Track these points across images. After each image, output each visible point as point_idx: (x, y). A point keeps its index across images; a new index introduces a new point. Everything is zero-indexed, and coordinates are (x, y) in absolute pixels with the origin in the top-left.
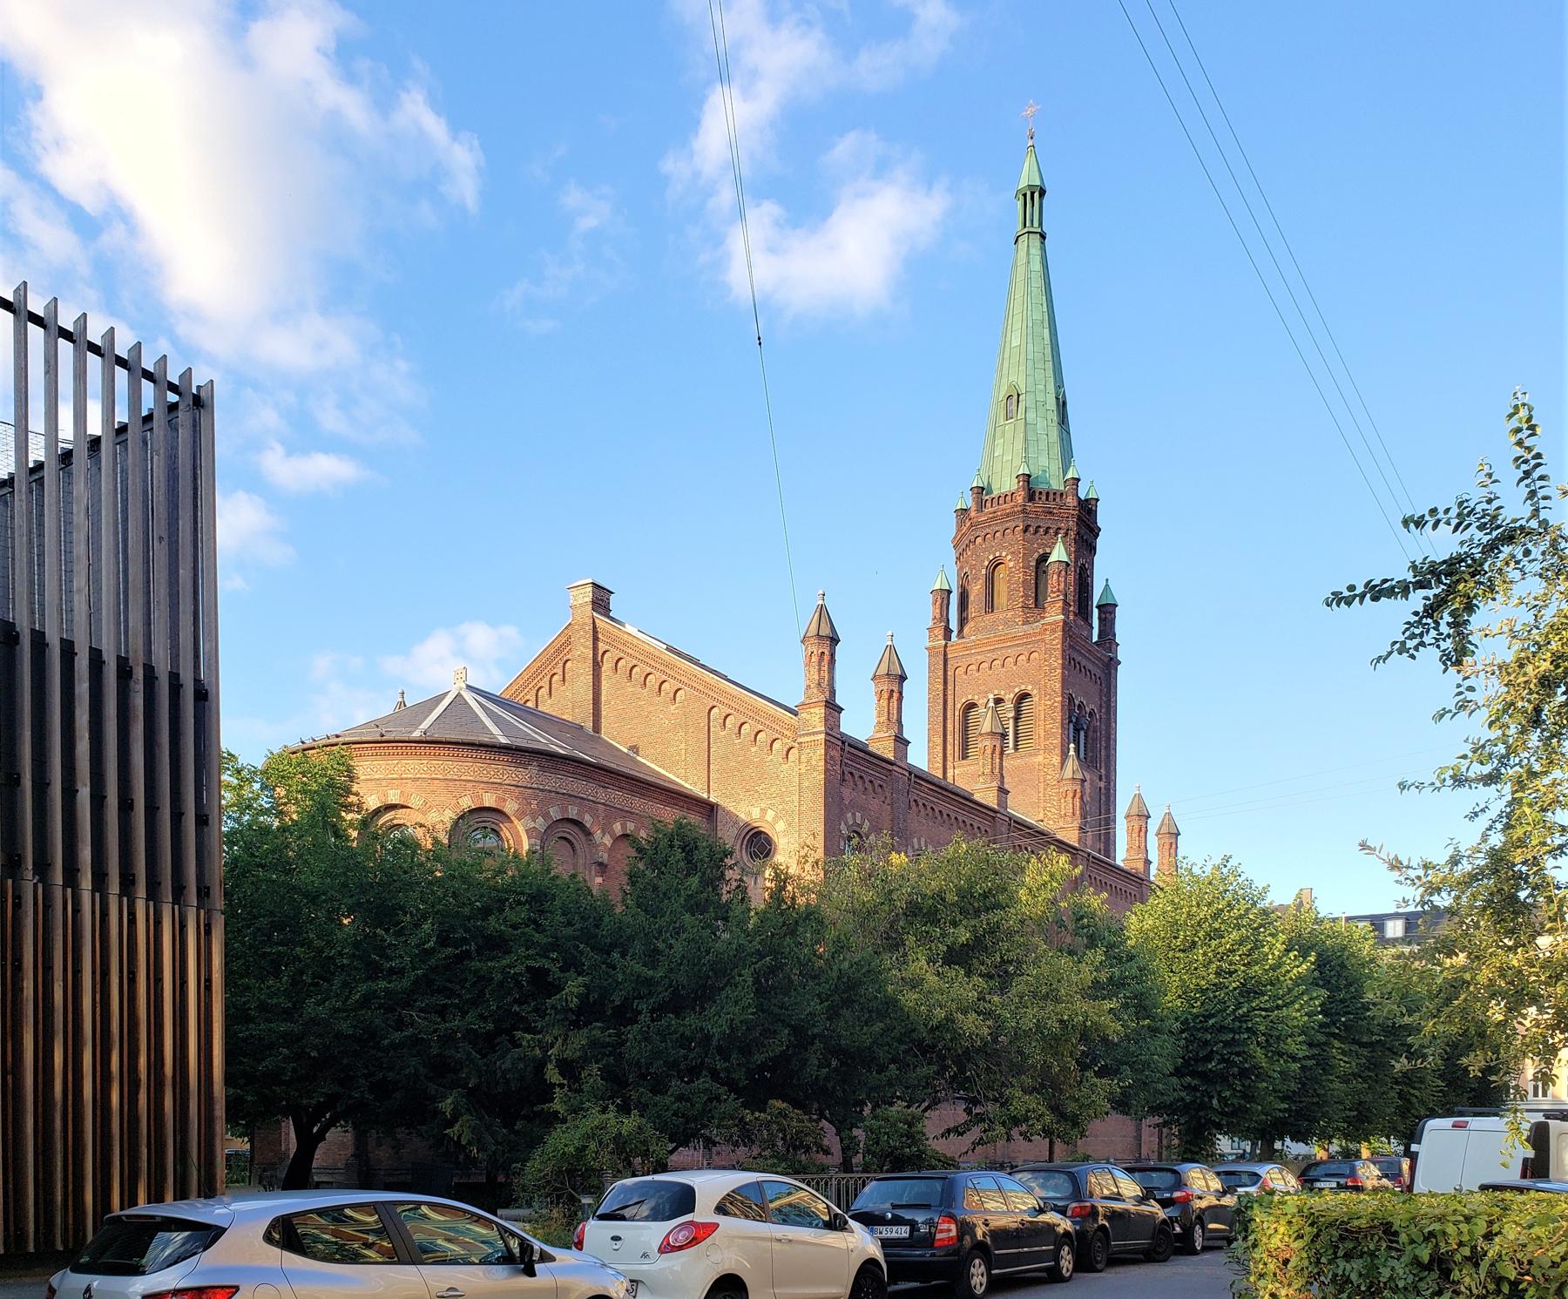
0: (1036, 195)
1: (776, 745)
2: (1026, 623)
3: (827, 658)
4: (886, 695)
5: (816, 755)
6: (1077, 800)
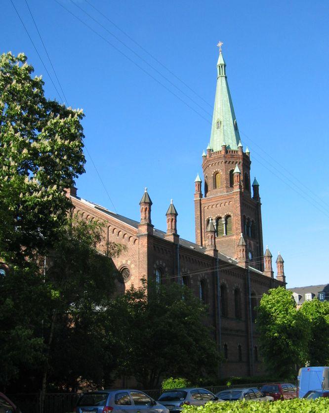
0: (223, 66)
1: (131, 239)
2: (227, 192)
3: (148, 209)
4: (170, 221)
5: (144, 241)
6: (244, 253)
